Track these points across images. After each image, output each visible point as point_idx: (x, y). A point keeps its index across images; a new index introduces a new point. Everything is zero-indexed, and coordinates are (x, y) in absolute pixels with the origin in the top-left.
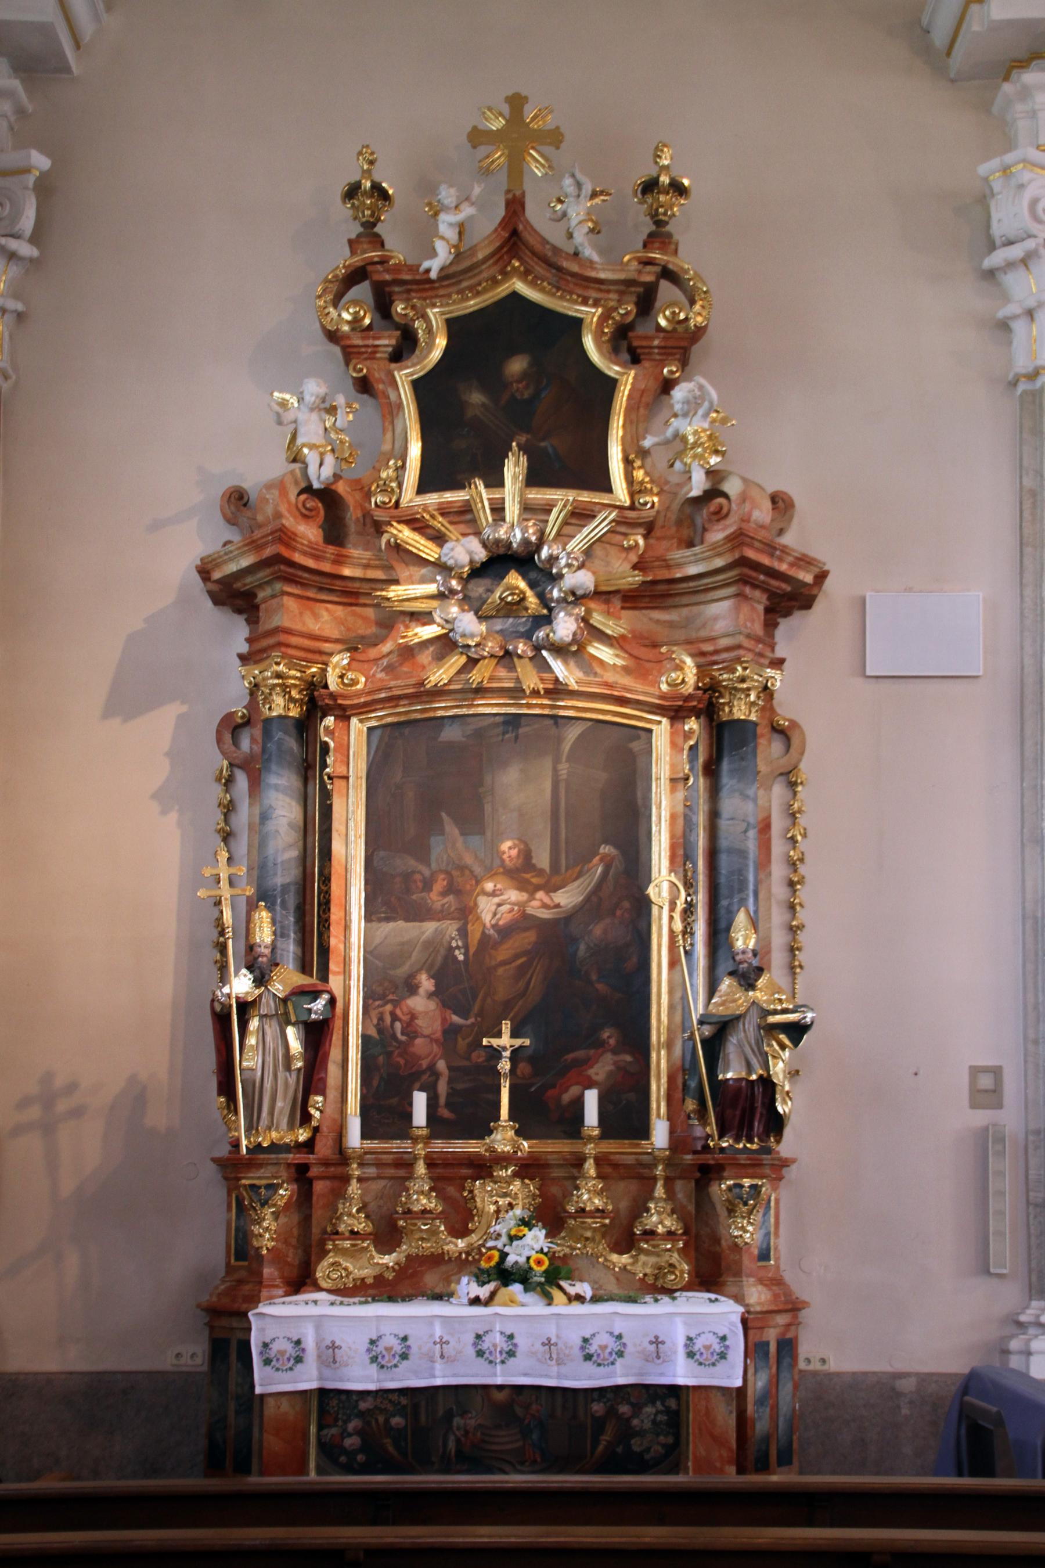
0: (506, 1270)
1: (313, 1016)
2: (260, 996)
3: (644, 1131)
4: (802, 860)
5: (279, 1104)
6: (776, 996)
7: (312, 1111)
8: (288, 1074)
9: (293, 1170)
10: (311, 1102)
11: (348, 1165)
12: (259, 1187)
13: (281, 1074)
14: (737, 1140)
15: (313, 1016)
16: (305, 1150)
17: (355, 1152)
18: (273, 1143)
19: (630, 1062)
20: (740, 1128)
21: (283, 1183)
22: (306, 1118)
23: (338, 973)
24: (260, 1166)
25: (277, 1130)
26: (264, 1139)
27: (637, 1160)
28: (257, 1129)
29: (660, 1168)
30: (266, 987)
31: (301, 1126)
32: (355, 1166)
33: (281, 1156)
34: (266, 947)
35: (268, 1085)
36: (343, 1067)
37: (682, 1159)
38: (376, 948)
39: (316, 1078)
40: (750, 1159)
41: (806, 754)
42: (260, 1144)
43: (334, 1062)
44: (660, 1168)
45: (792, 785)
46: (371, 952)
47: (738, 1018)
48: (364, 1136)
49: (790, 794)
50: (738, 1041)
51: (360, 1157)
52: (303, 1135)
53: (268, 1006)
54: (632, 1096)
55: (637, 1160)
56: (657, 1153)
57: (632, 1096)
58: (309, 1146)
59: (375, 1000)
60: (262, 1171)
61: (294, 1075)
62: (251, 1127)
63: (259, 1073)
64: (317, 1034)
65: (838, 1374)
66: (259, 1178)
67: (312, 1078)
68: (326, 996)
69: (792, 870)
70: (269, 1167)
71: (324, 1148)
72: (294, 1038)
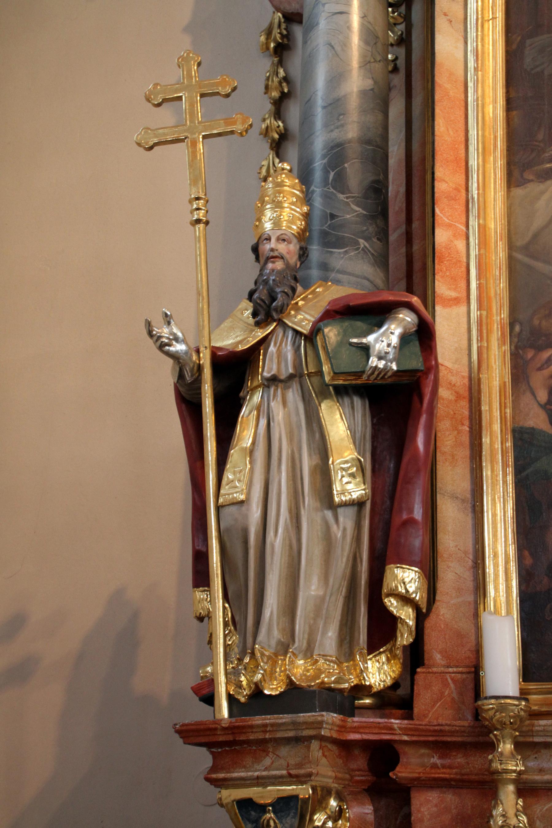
0: (307, 205)
1: (373, 361)
2: (264, 341)
5: (311, 588)
7: (392, 604)
8: (329, 514)
9: (360, 762)
10: (389, 583)
11: (492, 747)
12: (263, 808)
13: (311, 515)
15: (373, 361)
16: (399, 712)
17: (502, 708)
18: (292, 688)
21: (327, 792)
22: (382, 629)
23: (456, 301)
24: (263, 746)
25: (308, 652)
26: (270, 675)
28: (253, 654)
30: (280, 322)
31: (373, 647)
32: (506, 747)
33: (303, 717)
34: (281, 239)
35: (277, 541)
36: (474, 511)
38: (536, 236)
39: (397, 521)
42: (257, 692)
43: (454, 497)
46: (526, 249)
48: (528, 672)
51: (518, 723)
52: (378, 672)
53: (279, 358)
58: (396, 700)
59: (540, 349)
60: (267, 761)
61: (347, 519)
62: (244, 651)
63: (255, 513)
64: (395, 405)
65: (368, 764)
66: (260, 782)
67: (393, 523)
68: (407, 318)
70: (284, 751)
71: (435, 705)
72: (339, 424)
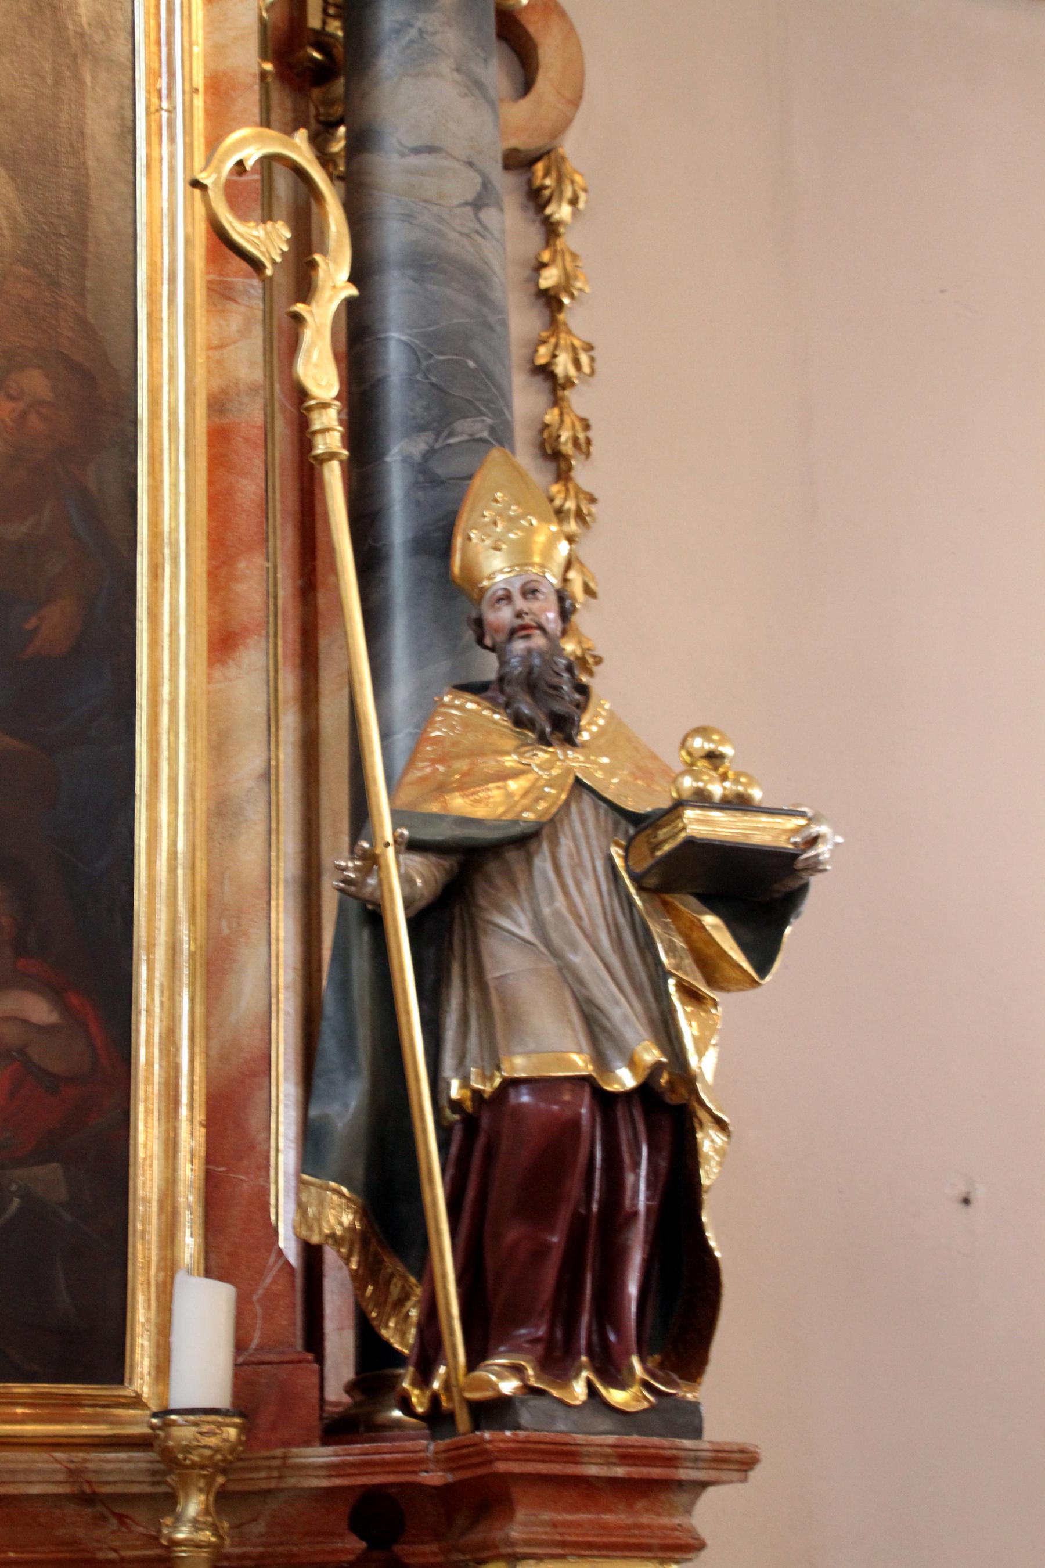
3: (91, 1344)
4: (584, 447)
6: (698, 743)
14: (556, 1362)
19: (42, 1029)
20: (565, 1312)
27: (74, 1474)
29: (193, 1506)
37: (285, 1468)
40: (626, 1457)
41: (584, 105)
44: (193, 1506)
45: (537, 199)
47: (524, 840)
49: (535, 234)
50: (539, 925)
54: (49, 1180)
55: (74, 1474)
56: (184, 1433)
57: (49, 1180)
69: (550, 476)
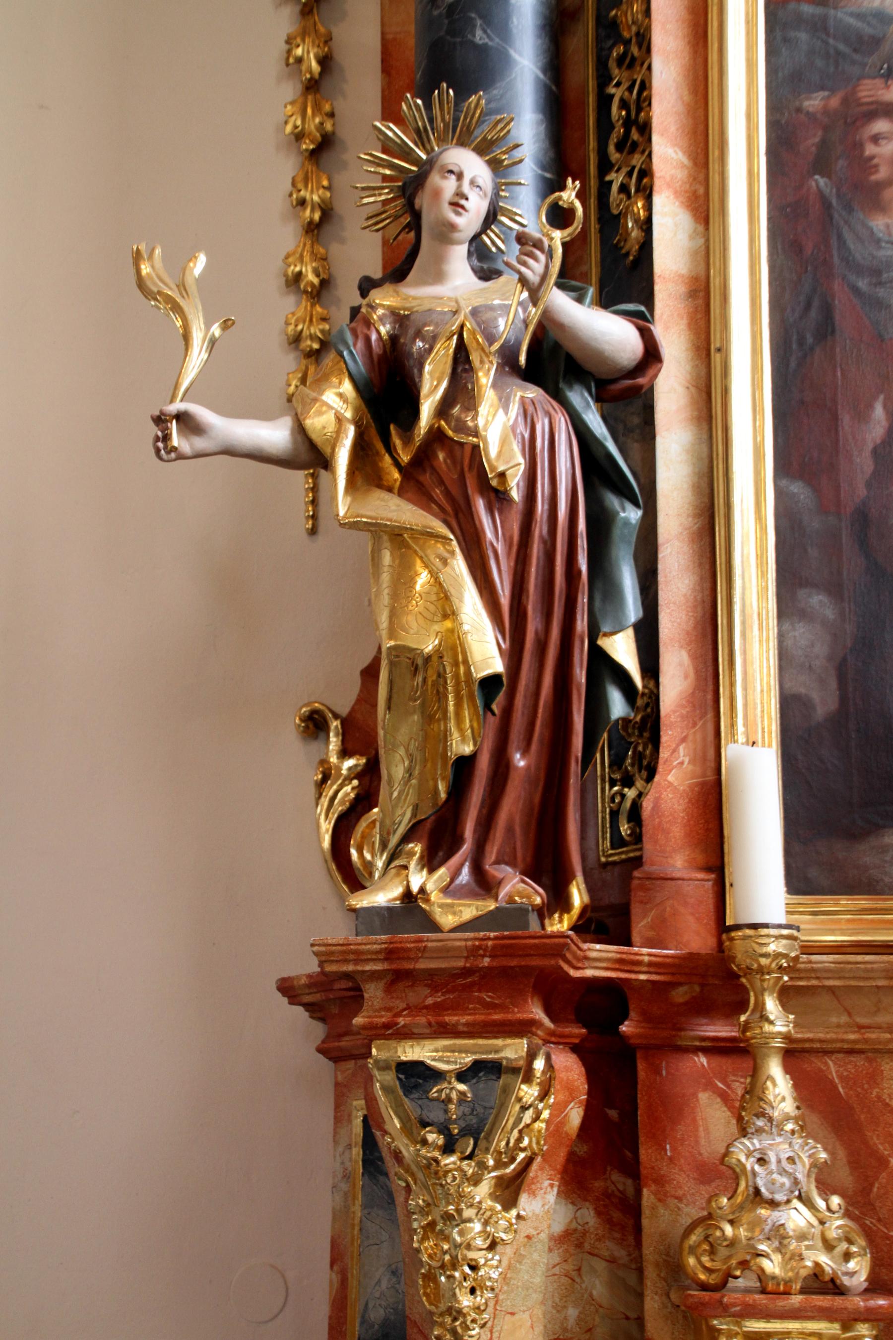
48: (798, 881)
